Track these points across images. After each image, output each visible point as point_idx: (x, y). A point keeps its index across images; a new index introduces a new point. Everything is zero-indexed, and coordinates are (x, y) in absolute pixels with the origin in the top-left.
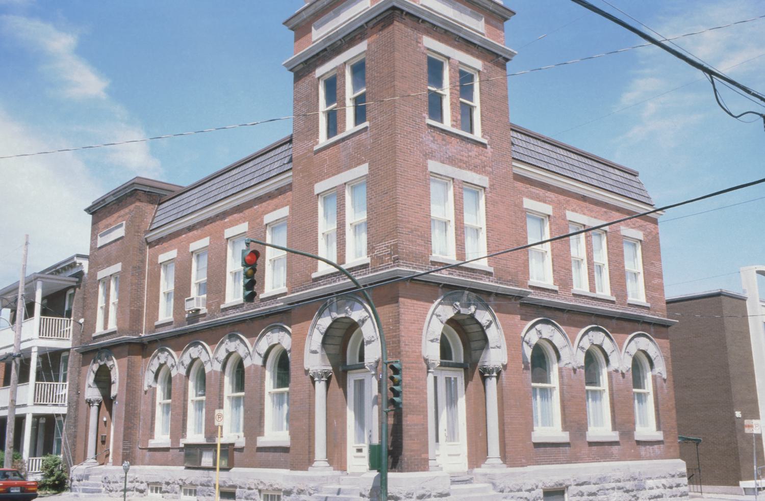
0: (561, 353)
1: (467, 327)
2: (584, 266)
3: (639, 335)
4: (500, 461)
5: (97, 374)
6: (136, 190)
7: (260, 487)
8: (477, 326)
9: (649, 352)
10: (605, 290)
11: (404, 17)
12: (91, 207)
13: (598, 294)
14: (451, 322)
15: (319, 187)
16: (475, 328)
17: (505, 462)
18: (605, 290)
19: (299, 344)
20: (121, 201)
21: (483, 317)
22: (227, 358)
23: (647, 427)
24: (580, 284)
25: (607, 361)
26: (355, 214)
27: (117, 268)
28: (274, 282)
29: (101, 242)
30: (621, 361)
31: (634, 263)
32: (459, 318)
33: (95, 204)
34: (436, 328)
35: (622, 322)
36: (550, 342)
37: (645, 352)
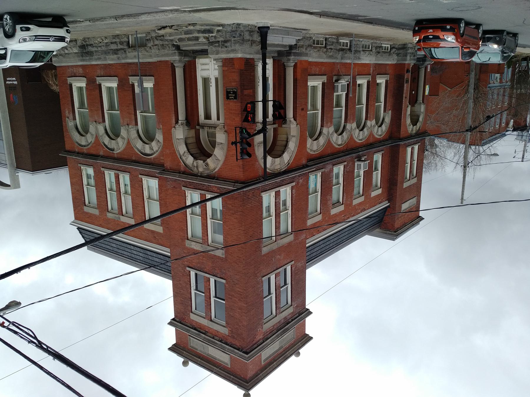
0: (136, 135)
1: (199, 152)
2: (122, 189)
3: (85, 146)
4: (175, 65)
5: (418, 120)
6: (395, 232)
7: (325, 50)
8: (192, 153)
9: (78, 135)
10: (109, 176)
11: (240, 347)
12: (421, 220)
13: (112, 173)
14: (209, 155)
15: (291, 238)
16: (194, 151)
17: (172, 64)
18: (109, 176)
19: (302, 143)
20: (403, 225)
21: (190, 160)
22: (343, 132)
23: (79, 84)
24: (125, 179)
25: (106, 130)
26: (268, 228)
27: (405, 185)
28: (315, 180)
29: (414, 201)
30: (98, 130)
31: (91, 195)
32: (204, 158)
33: (418, 223)
34: (219, 153)
35: (97, 156)
36: (144, 142)
37: (81, 135)
